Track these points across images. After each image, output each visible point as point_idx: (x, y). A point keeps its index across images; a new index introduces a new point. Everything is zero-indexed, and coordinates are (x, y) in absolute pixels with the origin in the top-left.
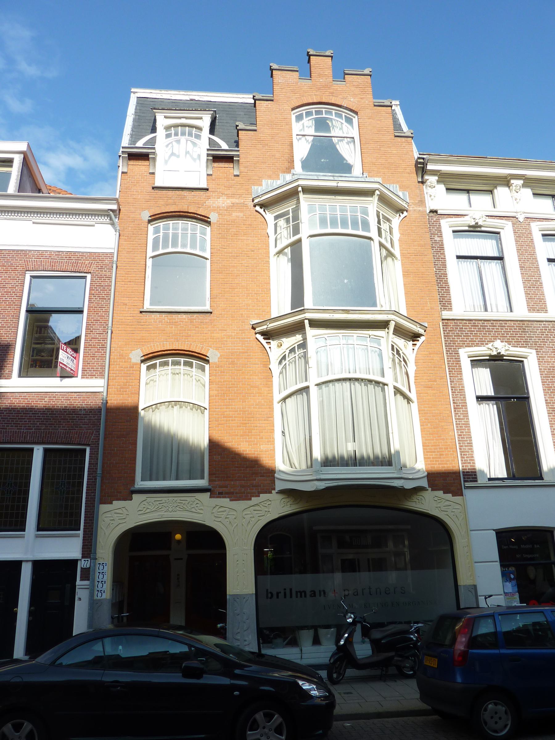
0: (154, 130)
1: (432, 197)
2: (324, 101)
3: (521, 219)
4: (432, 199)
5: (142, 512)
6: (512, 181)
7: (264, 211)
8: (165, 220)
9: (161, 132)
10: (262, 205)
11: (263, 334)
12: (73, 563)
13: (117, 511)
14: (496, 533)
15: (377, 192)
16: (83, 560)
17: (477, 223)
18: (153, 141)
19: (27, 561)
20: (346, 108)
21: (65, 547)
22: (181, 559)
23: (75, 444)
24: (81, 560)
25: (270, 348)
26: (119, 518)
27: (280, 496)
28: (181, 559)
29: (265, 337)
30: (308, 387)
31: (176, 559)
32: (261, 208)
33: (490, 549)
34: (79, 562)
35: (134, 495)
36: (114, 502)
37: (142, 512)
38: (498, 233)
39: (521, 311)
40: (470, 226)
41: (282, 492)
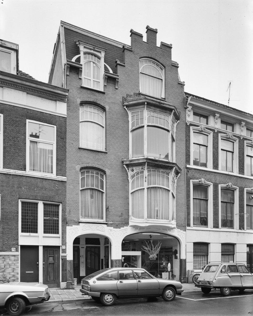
0: (78, 53)
1: (216, 123)
2: (153, 57)
3: (216, 131)
4: (242, 132)
5: (83, 230)
6: (216, 114)
7: (128, 109)
8: (101, 109)
9: (82, 55)
10: (127, 106)
11: (126, 165)
12: (58, 247)
13: (74, 229)
14: (221, 244)
15: (173, 111)
16: (63, 246)
17: (202, 130)
18: (78, 60)
19: (41, 246)
20: (161, 64)
21: (53, 240)
22: (84, 248)
23: (133, 209)
24: (62, 246)
25: (129, 171)
26: (73, 232)
27: (131, 228)
28: (84, 248)
29: (127, 166)
30: (144, 189)
31: (82, 248)
32: (126, 107)
33: (191, 248)
34: (61, 247)
35: (80, 224)
36: (73, 226)
37: (83, 230)
38: (208, 136)
39: (236, 173)
40: (199, 131)
41: (131, 226)
